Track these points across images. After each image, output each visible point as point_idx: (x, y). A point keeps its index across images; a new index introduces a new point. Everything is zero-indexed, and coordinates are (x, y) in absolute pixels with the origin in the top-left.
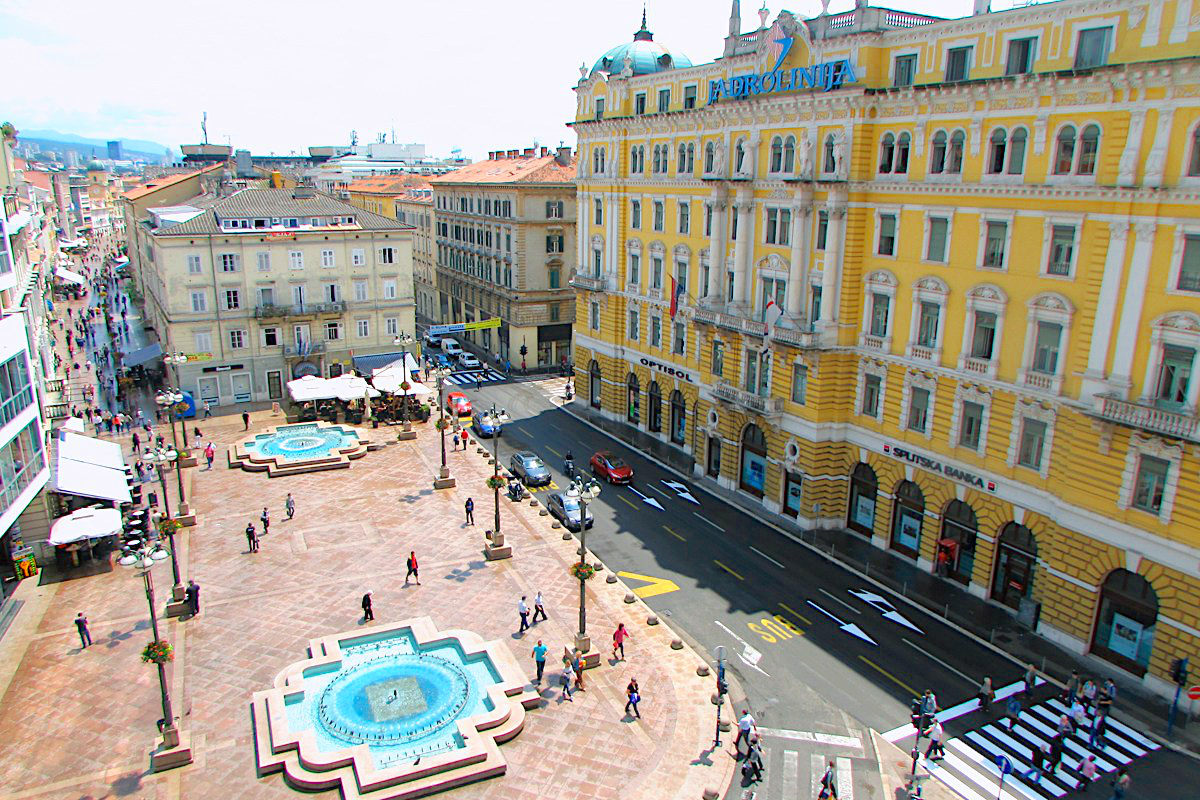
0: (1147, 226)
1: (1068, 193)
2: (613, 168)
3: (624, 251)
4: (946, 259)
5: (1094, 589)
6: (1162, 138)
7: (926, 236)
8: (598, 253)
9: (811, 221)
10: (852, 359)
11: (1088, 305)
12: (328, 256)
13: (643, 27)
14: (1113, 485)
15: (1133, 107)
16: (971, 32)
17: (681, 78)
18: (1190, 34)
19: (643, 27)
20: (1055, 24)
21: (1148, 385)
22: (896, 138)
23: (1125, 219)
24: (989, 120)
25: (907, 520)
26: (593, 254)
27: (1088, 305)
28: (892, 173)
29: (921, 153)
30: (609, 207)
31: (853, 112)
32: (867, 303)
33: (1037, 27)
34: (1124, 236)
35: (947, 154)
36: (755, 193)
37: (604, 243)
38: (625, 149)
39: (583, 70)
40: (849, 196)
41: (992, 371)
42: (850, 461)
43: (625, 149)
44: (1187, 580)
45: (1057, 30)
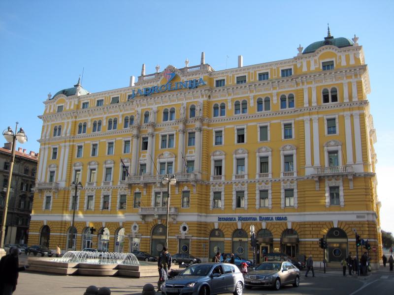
0: (307, 119)
1: (250, 117)
2: (48, 134)
3: (71, 168)
4: (269, 139)
5: (38, 233)
6: (49, 130)
7: (123, 146)
8: (52, 172)
9: (139, 141)
10: (208, 186)
11: (301, 145)
12: (59, 239)
13: (329, 34)
14: (347, 195)
15: (304, 87)
16: (118, 93)
17: (110, 94)
18: (316, 68)
19: (329, 34)
20: (230, 75)
21: (48, 181)
22: (330, 91)
23: (64, 144)
24: (256, 95)
25: (106, 237)
26: (49, 174)
27: (301, 145)
28: (169, 120)
29: (230, 107)
30: (63, 150)
31: (72, 117)
32: (74, 172)
33: (268, 69)
34: (309, 122)
35: (97, 125)
36: (155, 130)
37: (57, 167)
38: (75, 125)
39: (50, 96)
40: (203, 125)
41: (223, 178)
42: (68, 227)
43: (75, 125)
44: (354, 223)
45: (275, 70)
